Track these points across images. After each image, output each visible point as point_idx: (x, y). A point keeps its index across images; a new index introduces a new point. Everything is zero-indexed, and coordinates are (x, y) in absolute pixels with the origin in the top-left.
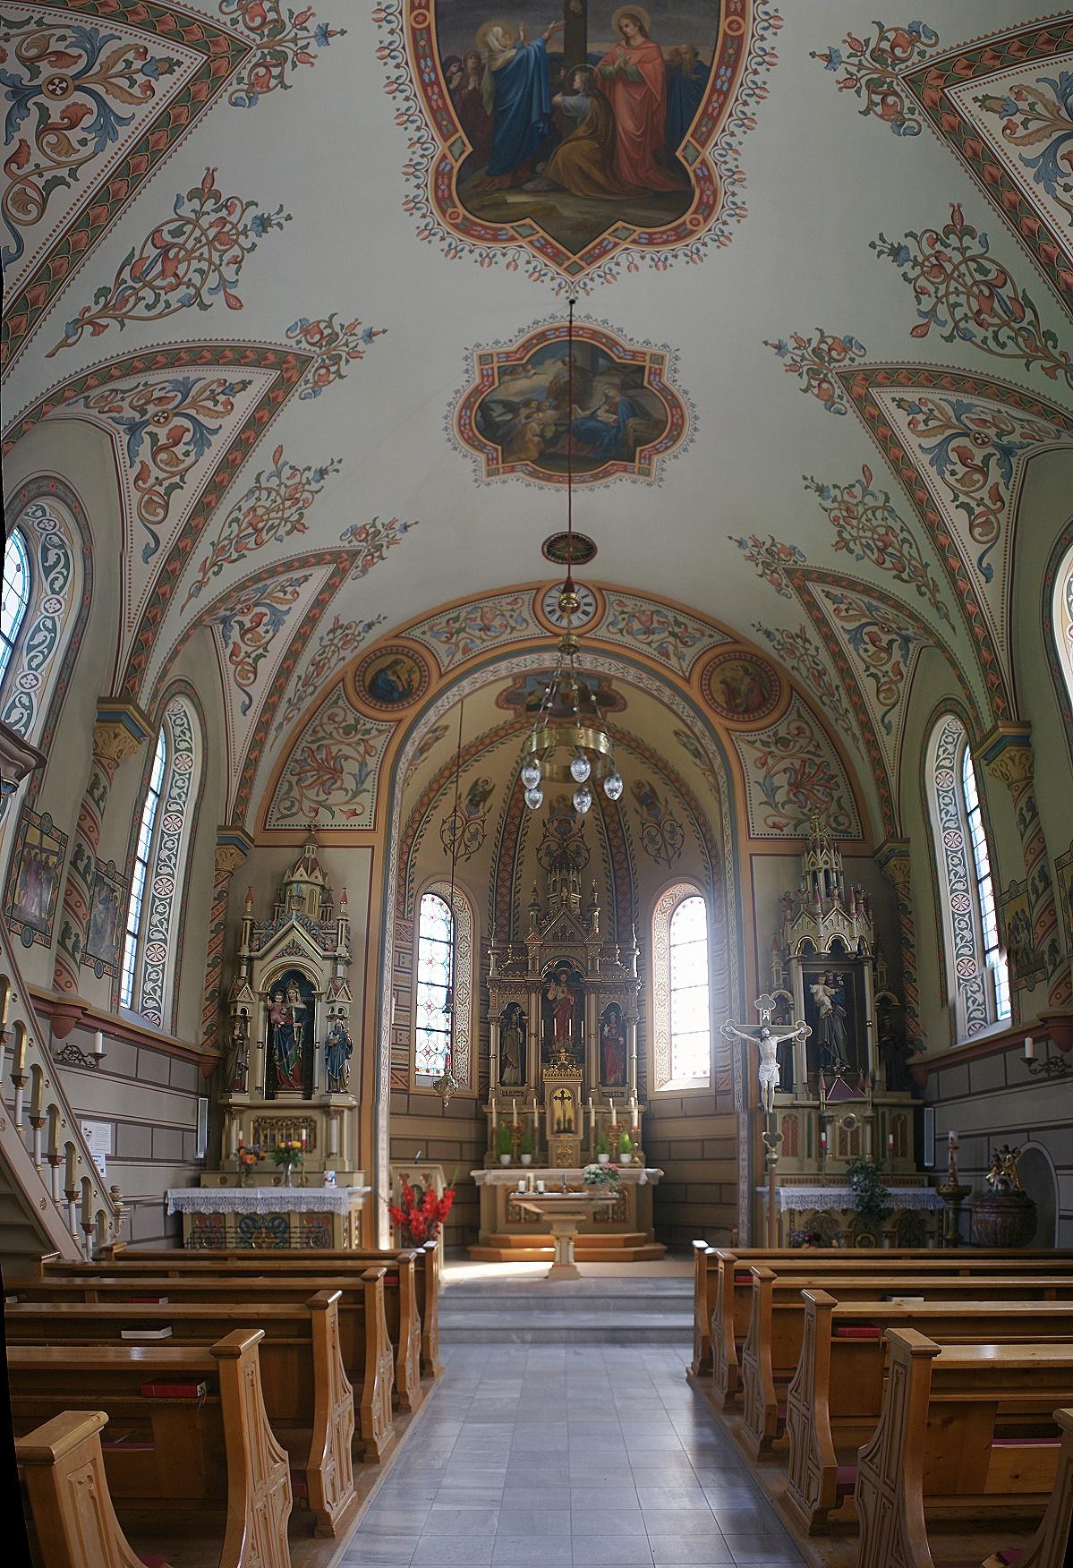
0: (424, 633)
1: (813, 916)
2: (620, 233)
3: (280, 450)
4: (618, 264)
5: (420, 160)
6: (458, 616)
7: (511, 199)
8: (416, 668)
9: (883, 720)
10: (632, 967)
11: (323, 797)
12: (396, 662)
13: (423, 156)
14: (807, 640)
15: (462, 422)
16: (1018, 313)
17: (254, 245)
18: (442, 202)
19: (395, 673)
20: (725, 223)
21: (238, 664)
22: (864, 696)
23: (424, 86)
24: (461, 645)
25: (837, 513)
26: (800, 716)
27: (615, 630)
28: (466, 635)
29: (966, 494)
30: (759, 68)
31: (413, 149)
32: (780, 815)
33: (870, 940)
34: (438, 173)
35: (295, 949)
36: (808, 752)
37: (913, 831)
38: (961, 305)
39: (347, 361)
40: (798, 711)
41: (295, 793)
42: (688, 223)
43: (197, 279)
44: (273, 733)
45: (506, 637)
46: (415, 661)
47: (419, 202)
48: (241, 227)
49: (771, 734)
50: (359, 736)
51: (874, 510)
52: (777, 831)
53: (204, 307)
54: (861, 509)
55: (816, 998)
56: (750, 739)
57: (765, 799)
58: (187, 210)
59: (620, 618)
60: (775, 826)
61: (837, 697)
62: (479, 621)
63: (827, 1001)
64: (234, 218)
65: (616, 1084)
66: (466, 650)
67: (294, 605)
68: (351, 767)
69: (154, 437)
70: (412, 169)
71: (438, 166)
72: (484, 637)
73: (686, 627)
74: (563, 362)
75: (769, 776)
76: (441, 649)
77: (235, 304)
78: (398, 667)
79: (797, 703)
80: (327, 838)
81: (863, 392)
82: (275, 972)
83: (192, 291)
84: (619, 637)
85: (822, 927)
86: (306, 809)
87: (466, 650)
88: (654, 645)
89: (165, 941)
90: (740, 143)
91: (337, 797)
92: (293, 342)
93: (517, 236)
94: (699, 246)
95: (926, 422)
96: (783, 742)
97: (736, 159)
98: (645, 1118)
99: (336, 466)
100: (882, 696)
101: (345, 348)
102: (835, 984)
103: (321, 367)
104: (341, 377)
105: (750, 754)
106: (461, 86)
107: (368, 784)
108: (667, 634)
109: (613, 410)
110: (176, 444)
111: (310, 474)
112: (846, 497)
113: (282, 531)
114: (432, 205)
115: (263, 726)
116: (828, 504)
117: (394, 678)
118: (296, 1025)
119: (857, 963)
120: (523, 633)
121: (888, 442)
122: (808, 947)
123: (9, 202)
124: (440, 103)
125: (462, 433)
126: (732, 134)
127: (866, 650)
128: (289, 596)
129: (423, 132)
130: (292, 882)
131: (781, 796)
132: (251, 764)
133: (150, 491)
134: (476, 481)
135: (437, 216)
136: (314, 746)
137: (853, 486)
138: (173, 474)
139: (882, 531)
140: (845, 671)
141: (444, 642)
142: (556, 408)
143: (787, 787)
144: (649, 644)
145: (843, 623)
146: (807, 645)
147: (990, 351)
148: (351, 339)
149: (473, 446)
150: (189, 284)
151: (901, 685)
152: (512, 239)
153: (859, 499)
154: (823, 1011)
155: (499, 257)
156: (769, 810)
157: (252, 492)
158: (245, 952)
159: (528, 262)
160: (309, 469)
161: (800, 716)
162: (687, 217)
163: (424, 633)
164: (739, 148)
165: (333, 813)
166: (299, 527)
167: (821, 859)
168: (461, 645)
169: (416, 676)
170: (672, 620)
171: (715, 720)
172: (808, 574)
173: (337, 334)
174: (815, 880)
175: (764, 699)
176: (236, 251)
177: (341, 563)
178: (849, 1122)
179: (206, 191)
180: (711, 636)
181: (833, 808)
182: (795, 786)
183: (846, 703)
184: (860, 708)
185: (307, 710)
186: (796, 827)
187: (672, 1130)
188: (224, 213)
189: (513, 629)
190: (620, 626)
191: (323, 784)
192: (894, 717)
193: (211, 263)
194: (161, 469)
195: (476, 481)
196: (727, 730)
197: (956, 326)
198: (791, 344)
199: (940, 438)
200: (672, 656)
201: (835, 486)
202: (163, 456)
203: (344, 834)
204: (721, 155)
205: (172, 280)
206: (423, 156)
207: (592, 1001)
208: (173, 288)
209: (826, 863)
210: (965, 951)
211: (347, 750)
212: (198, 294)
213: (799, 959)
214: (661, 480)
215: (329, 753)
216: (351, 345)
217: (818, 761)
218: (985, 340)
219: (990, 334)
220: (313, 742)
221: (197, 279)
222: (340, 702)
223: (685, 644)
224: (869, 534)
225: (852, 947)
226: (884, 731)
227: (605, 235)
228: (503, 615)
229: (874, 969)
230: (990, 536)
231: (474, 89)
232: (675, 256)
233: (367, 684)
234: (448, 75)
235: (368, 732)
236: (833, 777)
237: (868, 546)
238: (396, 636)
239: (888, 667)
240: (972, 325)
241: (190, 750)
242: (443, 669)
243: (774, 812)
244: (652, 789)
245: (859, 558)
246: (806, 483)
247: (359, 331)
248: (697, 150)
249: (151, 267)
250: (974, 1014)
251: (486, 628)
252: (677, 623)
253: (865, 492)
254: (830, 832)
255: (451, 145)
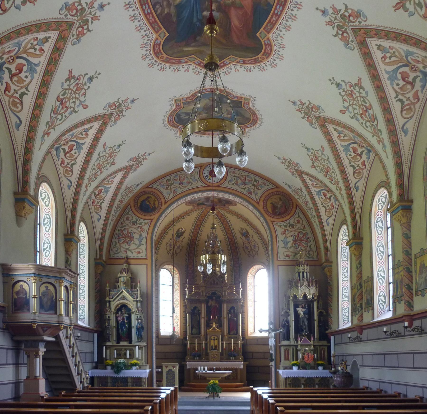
0: (158, 186)
1: (297, 287)
2: (231, 59)
3: (105, 144)
4: (231, 69)
5: (147, 42)
6: (170, 179)
7: (185, 49)
8: (156, 200)
9: (326, 221)
10: (239, 294)
11: (127, 247)
12: (149, 197)
13: (148, 40)
14: (302, 191)
15: (169, 120)
16: (373, 120)
17: (89, 87)
18: (157, 54)
19: (148, 201)
20: (275, 60)
21: (95, 206)
22: (321, 213)
23: (146, 15)
24: (172, 190)
25: (312, 157)
26: (299, 216)
27: (231, 184)
28: (174, 186)
29: (354, 162)
30: (294, 9)
31: (144, 38)
32: (289, 251)
33: (317, 294)
34: (155, 45)
35: (124, 298)
36: (301, 229)
37: (333, 259)
38: (356, 109)
39: (92, 22)
40: (298, 214)
41: (118, 245)
42: (259, 58)
43: (72, 105)
44: (108, 226)
45: (189, 187)
46: (155, 197)
47: (137, 16)
48: (84, 83)
49: (288, 223)
50: (138, 225)
51: (324, 160)
52: (288, 258)
53: (76, 112)
54: (320, 158)
55: (298, 312)
56: (281, 224)
57: (284, 246)
58: (65, 86)
59: (233, 179)
60: (287, 256)
61: (312, 211)
62: (178, 180)
63: (302, 313)
64: (81, 82)
65: (234, 334)
66: (174, 192)
67: (112, 185)
68: (136, 236)
69: (64, 150)
70: (144, 45)
71: (155, 42)
72: (181, 187)
73: (259, 182)
74: (210, 100)
75: (286, 238)
76: (165, 192)
77: (85, 107)
78: (150, 199)
79: (298, 211)
80: (132, 261)
81: (323, 124)
82: (118, 305)
83: (72, 109)
84: (233, 186)
85: (300, 291)
86: (123, 252)
87: (174, 192)
88: (246, 189)
89: (84, 298)
90: (284, 35)
91: (133, 247)
92: (106, 111)
93: (188, 61)
94: (264, 66)
95: (344, 137)
96: (292, 226)
97: (282, 40)
98: (243, 345)
99: (124, 142)
100: (327, 213)
101: (90, 15)
102: (305, 308)
103: (116, 115)
104: (90, 31)
105: (279, 230)
106: (162, 11)
107: (144, 242)
108: (251, 185)
109: (230, 113)
110: (71, 150)
111: (115, 148)
112: (316, 153)
113: (108, 166)
114: (153, 55)
115: (105, 225)
116: (310, 154)
117: (148, 203)
118: (126, 321)
119: (312, 301)
120: (196, 185)
121: (330, 141)
122: (295, 296)
123: (11, 106)
124: (153, 20)
125: (170, 124)
126: (281, 31)
127: (322, 198)
128: (110, 182)
129: (147, 32)
130: (121, 277)
131: (289, 245)
132: (102, 238)
133: (66, 167)
134: (176, 137)
135: (155, 59)
136: (123, 229)
137: (318, 151)
138: (72, 160)
139: (326, 167)
140: (315, 204)
141: (166, 189)
142: (206, 113)
143: (292, 242)
144: (244, 189)
145: (314, 188)
146: (302, 193)
147: (363, 127)
148: (92, 10)
149: (174, 127)
150: (71, 107)
151: (333, 210)
152: (186, 62)
153: (320, 155)
154: (301, 316)
155: (181, 68)
156: (286, 250)
157: (98, 159)
158: (107, 299)
159: (193, 69)
160: (115, 146)
161: (299, 216)
162: (260, 56)
163: (158, 186)
164: (283, 36)
165: (132, 253)
166: (113, 163)
167: (301, 268)
168: (172, 190)
169: (156, 203)
170: (253, 179)
171: (268, 218)
172: (302, 172)
173: (121, 104)
174: (299, 276)
175: (286, 209)
176: (83, 91)
177: (127, 170)
178: (305, 350)
179: (71, 77)
180: (268, 185)
181: (308, 248)
182: (295, 241)
183: (314, 214)
184: (319, 216)
185: (118, 216)
186: (294, 256)
187: (251, 349)
188: (77, 81)
189: (192, 183)
190: (233, 182)
191: (127, 242)
192: (331, 221)
193: (76, 98)
194: (69, 160)
195: (176, 137)
196: (272, 221)
197: (355, 114)
198: (299, 103)
199: (348, 143)
200: (253, 193)
201: (312, 149)
202: (68, 155)
203: (139, 260)
204: (276, 37)
205: (66, 109)
206: (148, 40)
207: (225, 306)
208: (66, 111)
209: (303, 269)
210: (346, 299)
211: (134, 230)
212: (74, 109)
213: (292, 300)
214: (249, 136)
215: (128, 231)
216: (93, 13)
217: (304, 232)
218: (362, 123)
219: (364, 122)
220: (122, 227)
221: (72, 105)
222: (130, 213)
223: (258, 189)
224: (322, 166)
225: (310, 297)
226: (327, 225)
227: (225, 59)
228: (188, 178)
229: (318, 303)
230: (360, 177)
231: (168, 13)
232: (255, 68)
233: (139, 205)
234: (156, 9)
235: (141, 224)
236: (309, 238)
237: (322, 170)
238: (148, 187)
239: (329, 204)
240: (359, 117)
241: (84, 237)
242: (166, 200)
243: (286, 250)
244: (247, 231)
245: (319, 173)
246: (302, 145)
247: (129, 101)
248: (265, 34)
249: (59, 108)
250: (345, 319)
251: (181, 183)
252: (255, 180)
253: (322, 154)
254: (306, 257)
255: (160, 34)
